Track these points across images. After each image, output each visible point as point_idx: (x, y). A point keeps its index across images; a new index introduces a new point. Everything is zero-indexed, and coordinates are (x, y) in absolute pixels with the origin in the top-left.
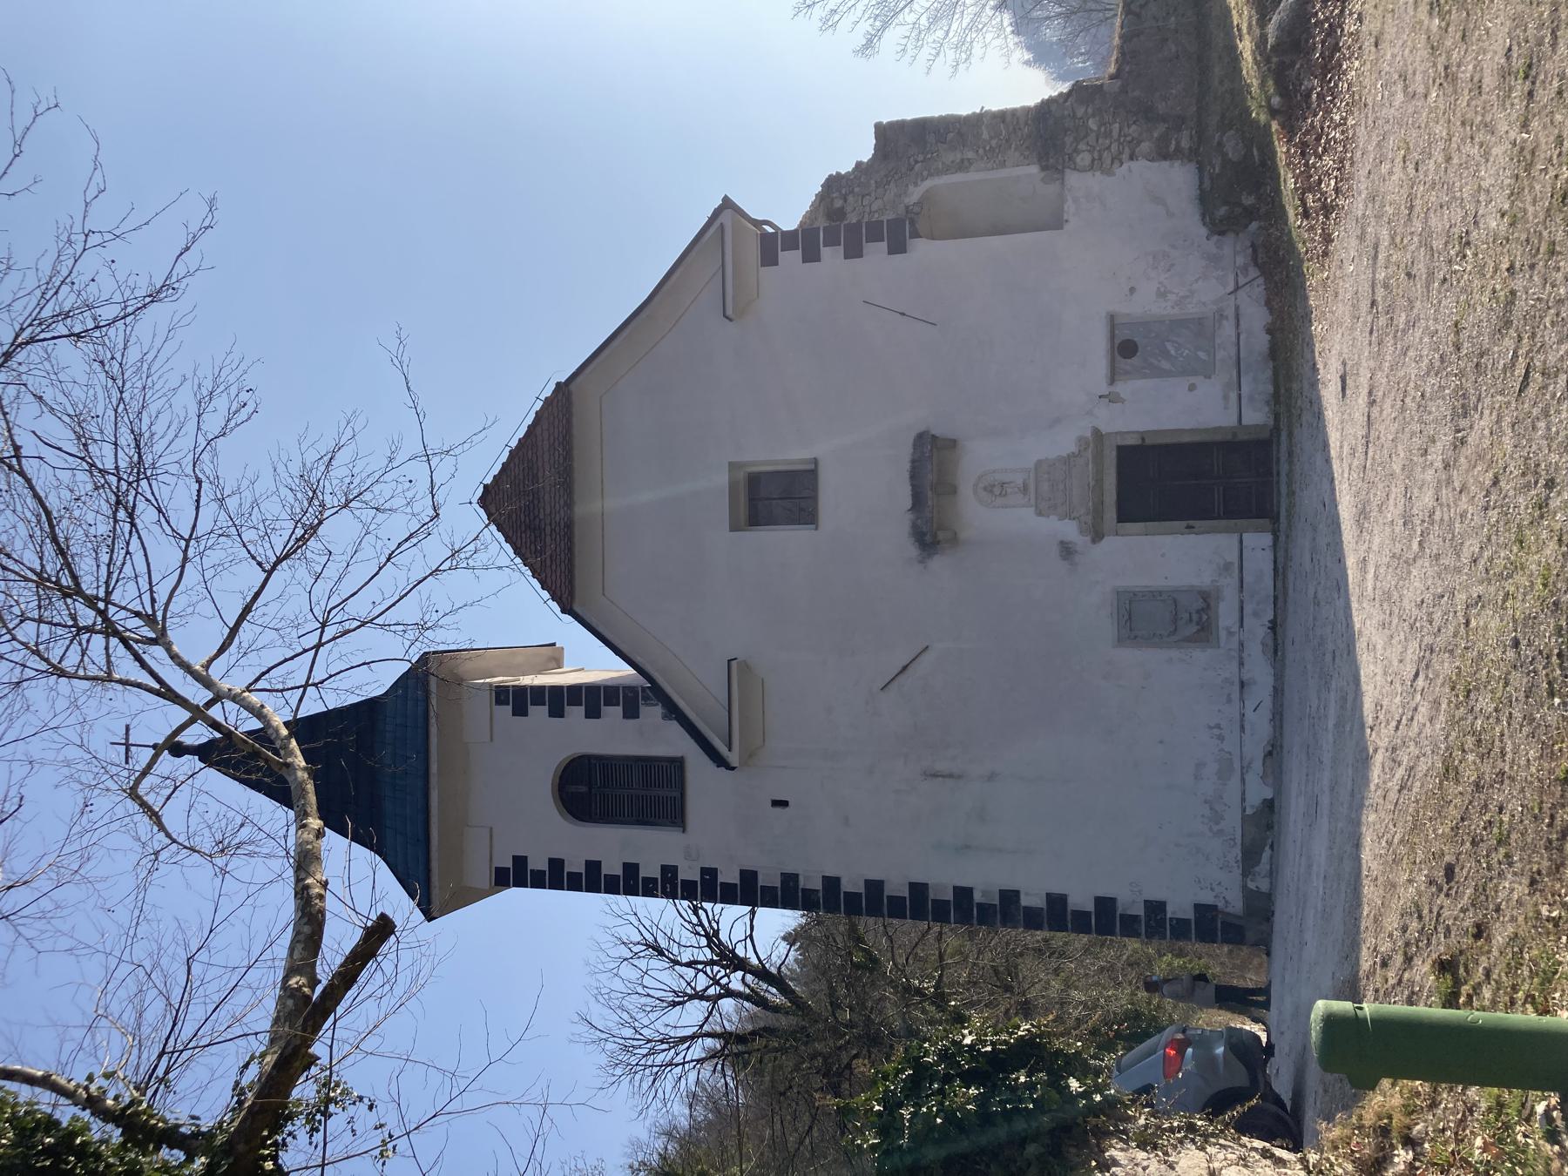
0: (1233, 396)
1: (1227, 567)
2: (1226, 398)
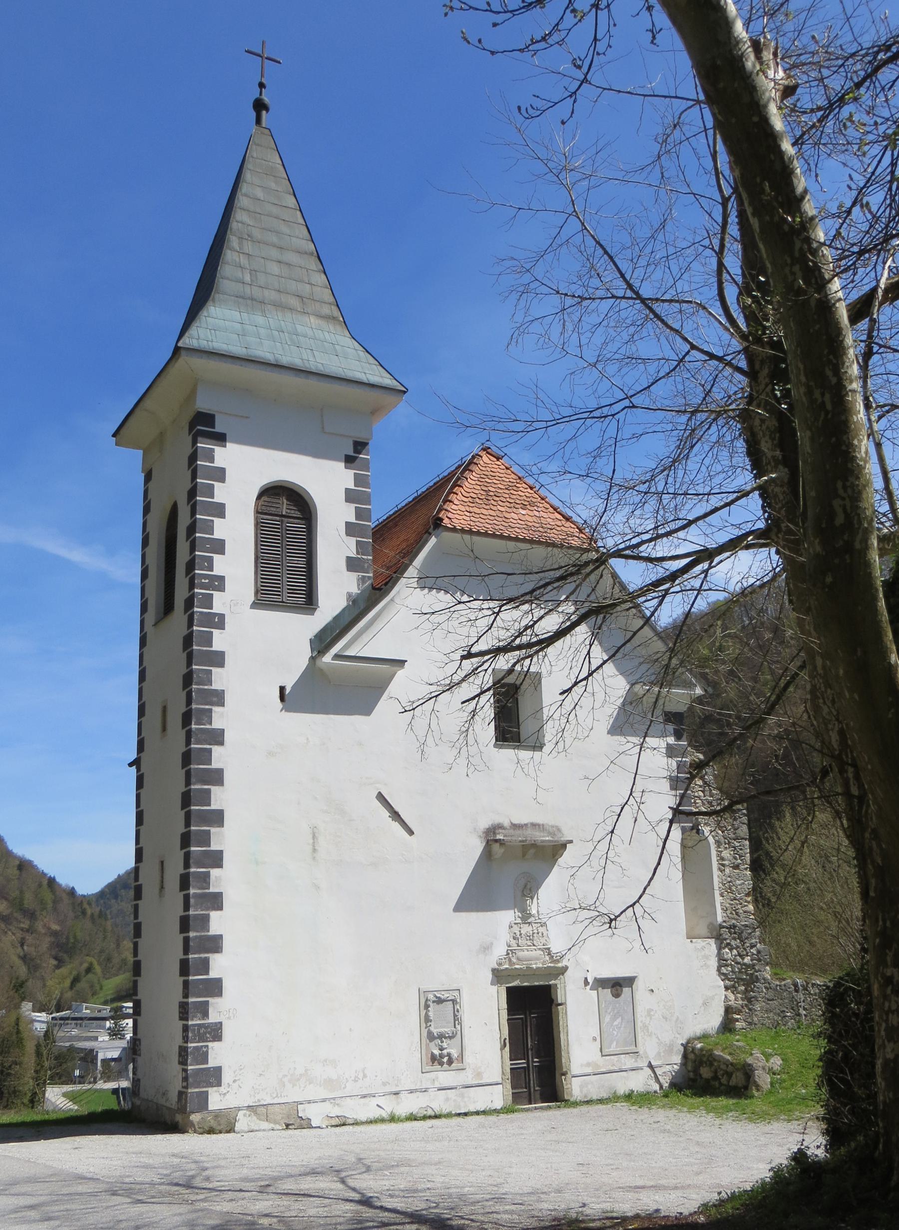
0: (589, 1070)
1: (479, 1075)
2: (588, 1065)
